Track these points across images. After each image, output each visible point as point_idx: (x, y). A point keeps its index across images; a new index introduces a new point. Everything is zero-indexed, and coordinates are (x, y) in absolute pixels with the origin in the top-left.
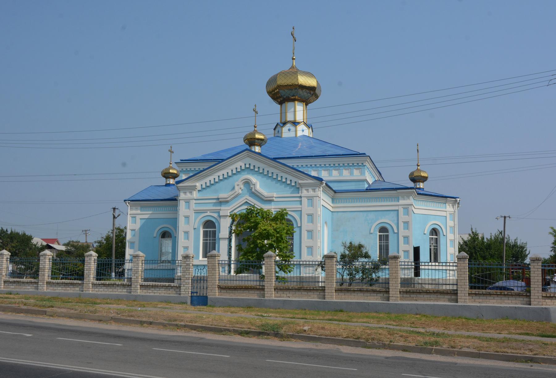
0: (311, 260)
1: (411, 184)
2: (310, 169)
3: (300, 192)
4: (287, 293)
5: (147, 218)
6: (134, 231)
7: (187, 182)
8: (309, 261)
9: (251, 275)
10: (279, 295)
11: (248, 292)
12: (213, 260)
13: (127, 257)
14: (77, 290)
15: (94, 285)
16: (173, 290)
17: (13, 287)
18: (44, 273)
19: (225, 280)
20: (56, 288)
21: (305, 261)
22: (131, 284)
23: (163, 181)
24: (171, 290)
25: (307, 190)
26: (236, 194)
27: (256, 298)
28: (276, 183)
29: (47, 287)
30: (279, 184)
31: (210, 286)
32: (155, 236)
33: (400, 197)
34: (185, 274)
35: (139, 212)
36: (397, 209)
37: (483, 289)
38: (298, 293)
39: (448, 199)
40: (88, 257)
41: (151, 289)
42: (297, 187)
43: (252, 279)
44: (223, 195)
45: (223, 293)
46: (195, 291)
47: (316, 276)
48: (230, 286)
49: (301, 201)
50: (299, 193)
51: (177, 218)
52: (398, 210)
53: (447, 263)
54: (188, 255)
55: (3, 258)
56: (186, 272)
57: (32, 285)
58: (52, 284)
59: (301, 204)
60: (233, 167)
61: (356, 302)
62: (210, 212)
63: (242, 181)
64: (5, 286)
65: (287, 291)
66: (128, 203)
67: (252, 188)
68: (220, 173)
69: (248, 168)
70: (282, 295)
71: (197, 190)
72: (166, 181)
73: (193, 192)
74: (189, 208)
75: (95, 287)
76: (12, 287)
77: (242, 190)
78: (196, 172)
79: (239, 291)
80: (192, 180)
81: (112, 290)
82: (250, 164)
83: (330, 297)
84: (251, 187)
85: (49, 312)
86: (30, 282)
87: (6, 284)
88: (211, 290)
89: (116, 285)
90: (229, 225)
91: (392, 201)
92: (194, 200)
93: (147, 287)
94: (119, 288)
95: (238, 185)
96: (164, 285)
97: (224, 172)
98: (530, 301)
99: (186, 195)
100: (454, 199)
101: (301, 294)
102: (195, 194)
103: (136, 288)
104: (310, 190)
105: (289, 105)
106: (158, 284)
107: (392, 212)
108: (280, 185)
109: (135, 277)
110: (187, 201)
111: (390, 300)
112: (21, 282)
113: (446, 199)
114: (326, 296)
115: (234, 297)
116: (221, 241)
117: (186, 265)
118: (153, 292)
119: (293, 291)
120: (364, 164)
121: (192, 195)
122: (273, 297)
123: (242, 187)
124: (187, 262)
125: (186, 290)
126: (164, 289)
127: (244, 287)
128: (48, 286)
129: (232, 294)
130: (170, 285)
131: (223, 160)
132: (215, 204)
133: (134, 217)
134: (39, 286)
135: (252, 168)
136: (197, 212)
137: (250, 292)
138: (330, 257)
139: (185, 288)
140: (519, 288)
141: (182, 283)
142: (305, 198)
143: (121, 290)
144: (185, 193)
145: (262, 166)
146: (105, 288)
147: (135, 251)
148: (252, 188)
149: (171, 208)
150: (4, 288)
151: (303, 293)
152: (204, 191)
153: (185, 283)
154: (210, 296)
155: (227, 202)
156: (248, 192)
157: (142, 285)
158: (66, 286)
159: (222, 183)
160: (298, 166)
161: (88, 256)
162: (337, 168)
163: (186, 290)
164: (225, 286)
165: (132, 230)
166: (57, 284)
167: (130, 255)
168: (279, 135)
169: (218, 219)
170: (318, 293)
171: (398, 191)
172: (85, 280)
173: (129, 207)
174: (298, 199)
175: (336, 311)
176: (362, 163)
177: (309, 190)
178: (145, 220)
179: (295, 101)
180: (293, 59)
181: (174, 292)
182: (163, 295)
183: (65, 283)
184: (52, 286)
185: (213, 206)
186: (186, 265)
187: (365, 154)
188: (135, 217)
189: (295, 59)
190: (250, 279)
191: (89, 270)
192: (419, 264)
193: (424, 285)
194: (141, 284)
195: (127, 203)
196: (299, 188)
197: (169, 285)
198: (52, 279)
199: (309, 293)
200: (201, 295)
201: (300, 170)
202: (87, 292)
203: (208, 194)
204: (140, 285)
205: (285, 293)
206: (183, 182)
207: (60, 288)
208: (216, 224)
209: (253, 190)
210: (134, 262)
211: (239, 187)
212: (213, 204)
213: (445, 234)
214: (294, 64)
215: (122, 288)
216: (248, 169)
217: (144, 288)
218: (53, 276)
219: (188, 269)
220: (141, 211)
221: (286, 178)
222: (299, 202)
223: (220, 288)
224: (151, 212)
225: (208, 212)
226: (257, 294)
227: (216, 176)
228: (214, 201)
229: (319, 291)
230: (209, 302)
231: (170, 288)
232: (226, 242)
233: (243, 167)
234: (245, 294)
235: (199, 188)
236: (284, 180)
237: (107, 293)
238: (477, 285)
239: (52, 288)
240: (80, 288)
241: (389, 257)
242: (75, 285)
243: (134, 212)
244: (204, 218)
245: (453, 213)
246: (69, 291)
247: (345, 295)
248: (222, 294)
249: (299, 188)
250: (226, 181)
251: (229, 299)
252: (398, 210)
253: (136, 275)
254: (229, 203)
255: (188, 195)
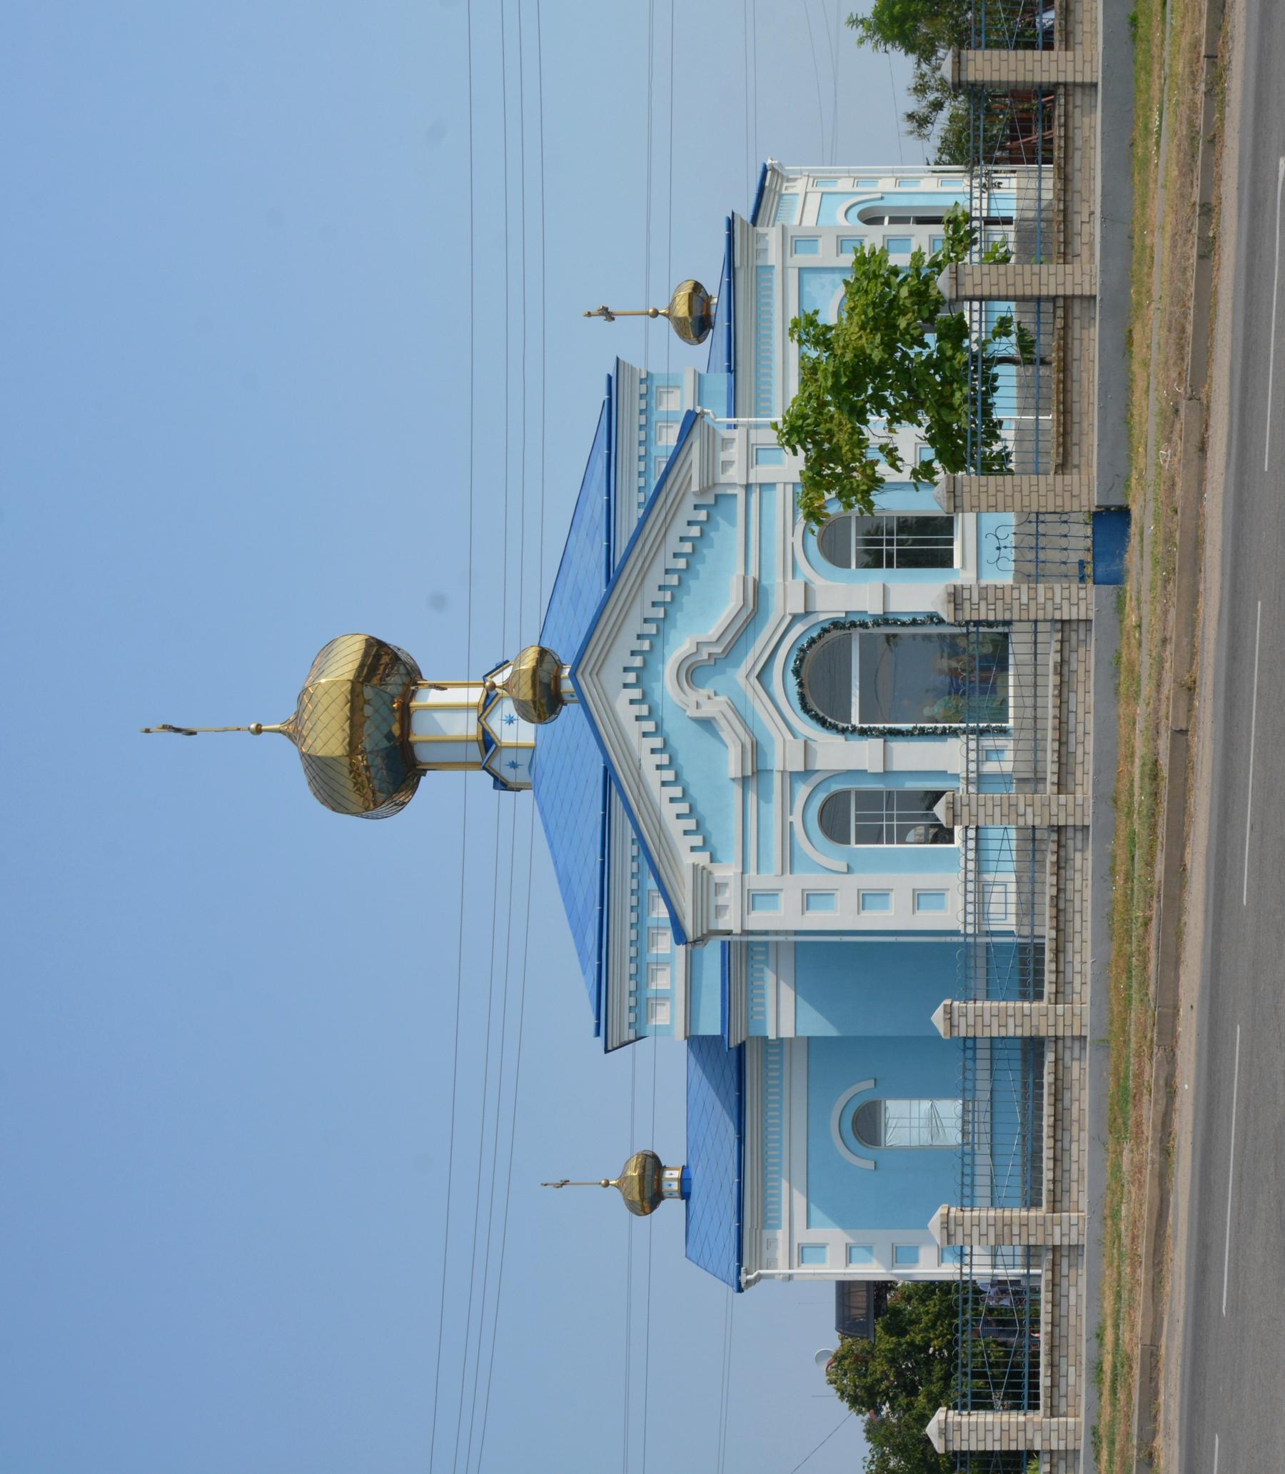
0: (961, 900)
1: (718, 334)
2: (654, 451)
3: (730, 491)
4: (1077, 219)
5: (804, 1200)
6: (854, 1251)
7: (678, 901)
8: (966, 881)
9: (1010, 651)
10: (1086, 248)
11: (1076, 364)
12: (966, 489)
13: (948, 1271)
14: (1080, 1071)
15: (1060, 996)
16: (1074, 656)
17: (1072, 1369)
18: (1016, 1221)
19: (1035, 708)
20: (1075, 1167)
21: (967, 744)
22: (1045, 1452)
23: (671, 1208)
24: (1074, 666)
25: (727, 464)
26: (730, 715)
27: (1095, 332)
28: (697, 578)
29: (1068, 1211)
30: (699, 567)
31: (1059, 502)
32: (871, 1165)
33: (760, 263)
34: (1016, 603)
35: (781, 1235)
36: (796, 271)
37: (1038, 1373)
38: (1078, 183)
39: (767, 184)
40: (956, 1023)
41: (1071, 749)
42: (712, 501)
43: (1029, 648)
44: (732, 765)
45: (1080, 456)
46: (1073, 569)
47: (1014, 847)
48: (1058, 427)
49: (761, 485)
50: (735, 496)
51: (808, 1037)
52: (800, 269)
53: (967, 778)
54: (949, 594)
55: (960, 1424)
56: (1008, 600)
57: (1064, 1282)
58: (1059, 1185)
59: (772, 485)
60: (633, 730)
61: (1102, 111)
62: (791, 814)
63: (681, 688)
64: (1071, 1410)
65: (1072, 222)
66: (747, 1273)
67: (710, 655)
68: (653, 778)
69: (638, 678)
70: (1085, 240)
71: (710, 867)
72: (671, 1195)
73: (717, 881)
74: (773, 894)
75: (1068, 988)
76: (1072, 1379)
77: (716, 694)
78: (646, 867)
79: (1076, 398)
80: (672, 879)
81: (1078, 916)
82: (626, 670)
83: (1088, 65)
84: (706, 657)
85: (1175, 720)
86: (1053, 1291)
87: (1063, 1409)
88: (1072, 496)
89: (1057, 897)
90: (839, 739)
91: (770, 289)
92: (746, 876)
93: (1064, 767)
94: (1070, 886)
95: (698, 705)
96: (1056, 692)
97: (649, 762)
98: (1082, 297)
99: (726, 907)
100: (769, 173)
101: (1080, 170)
102: (727, 871)
103: (1062, 1429)
104: (721, 900)
105: (421, 730)
106: (1055, 717)
107: (807, 289)
108: (704, 562)
109: (1029, 810)
110: (751, 900)
111: (1095, 80)
112: (1052, 1332)
113: (766, 191)
114: (1079, 823)
115: (1093, 417)
116: (896, 767)
117: (983, 604)
118: (1081, 739)
119: (1072, 200)
120: (644, 376)
121: (726, 885)
122: (1078, 1419)
123: (704, 692)
124: (975, 599)
125: (1074, 600)
126: (1072, 695)
127: (1061, 375)
128: (1065, 1204)
129: (1085, 424)
130: (1055, 667)
131: (609, 776)
132: (764, 796)
133: (801, 1253)
134: (1066, 1242)
135: (637, 662)
136: (790, 861)
137: (1076, 353)
138: (959, 62)
139: (1065, 604)
140: (1038, 640)
141: (1046, 824)
142: (752, 472)
143: (1078, 875)
144: (720, 910)
145: (634, 625)
146: (1069, 946)
147: (930, 1240)
148: (710, 655)
149: (770, 1066)
150: (1076, 1416)
151: (1077, 164)
152: (714, 840)
153: (1049, 603)
154: (1091, 499)
155: (756, 746)
156: (723, 673)
157: (1059, 784)
158: (1066, 1124)
159: (687, 776)
160: (640, 489)
161: (952, 1026)
162: (652, 465)
163: (1074, 600)
164: (1058, 446)
165: (849, 1260)
166: (1059, 1164)
167: (941, 1260)
168: (523, 759)
169: (816, 779)
170: (1078, 111)
171: (737, 264)
172: (1043, 1033)
173: (762, 1272)
174: (754, 498)
175: (1134, 37)
176: (642, 381)
177: (719, 903)
178: (813, 1207)
179: (408, 708)
180: (259, 730)
181: (1082, 650)
182: (1091, 699)
183: (1055, 1127)
184: (1066, 1186)
185: (768, 801)
186: (983, 604)
187: (610, 378)
188: (802, 1248)
189: (259, 726)
190: (1029, 658)
191: (1003, 1015)
192: (967, 1282)
193: (1044, 204)
194: (1055, 788)
195: (749, 1277)
196: (717, 497)
197: (1055, 673)
198: (1036, 1407)
199: (1078, 143)
200: (1089, 543)
201: (654, 484)
202: (1087, 1019)
203: (728, 829)
204: (1059, 793)
205: (1077, 226)
206: (680, 916)
207: (1075, 1147)
208: (836, 787)
209: (718, 650)
210: (973, 818)
211: (703, 700)
212: (762, 803)
213: (879, 195)
214: (277, 726)
215: (1070, 873)
216: (642, 676)
217: (1070, 777)
218: (1025, 1402)
219: (999, 595)
220: (779, 1226)
221: (682, 539)
222: (765, 494)
223: (1063, 466)
224: (785, 1185)
225: (790, 819)
226: (1082, 328)
227: (662, 796)
228: (752, 798)
229: (1070, 107)
230: (1114, 501)
231: (1066, 668)
232: (898, 746)
233: (636, 693)
234: (1085, 375)
235: (702, 858)
236: (687, 548)
237: (1088, 935)
238: (1026, 1391)
239: (1074, 1185)
240: (1072, 1059)
241: (948, 1037)
242: (1059, 1083)
243: (781, 1253)
244: (811, 833)
245: (811, 180)
246: (1086, 1106)
247: (1081, 22)
248: (1083, 460)
249: (717, 497)
250: (681, 759)
251: (1102, 420)
252: (801, 270)
253: (1021, 811)
254: (761, 741)
255: (730, 897)
